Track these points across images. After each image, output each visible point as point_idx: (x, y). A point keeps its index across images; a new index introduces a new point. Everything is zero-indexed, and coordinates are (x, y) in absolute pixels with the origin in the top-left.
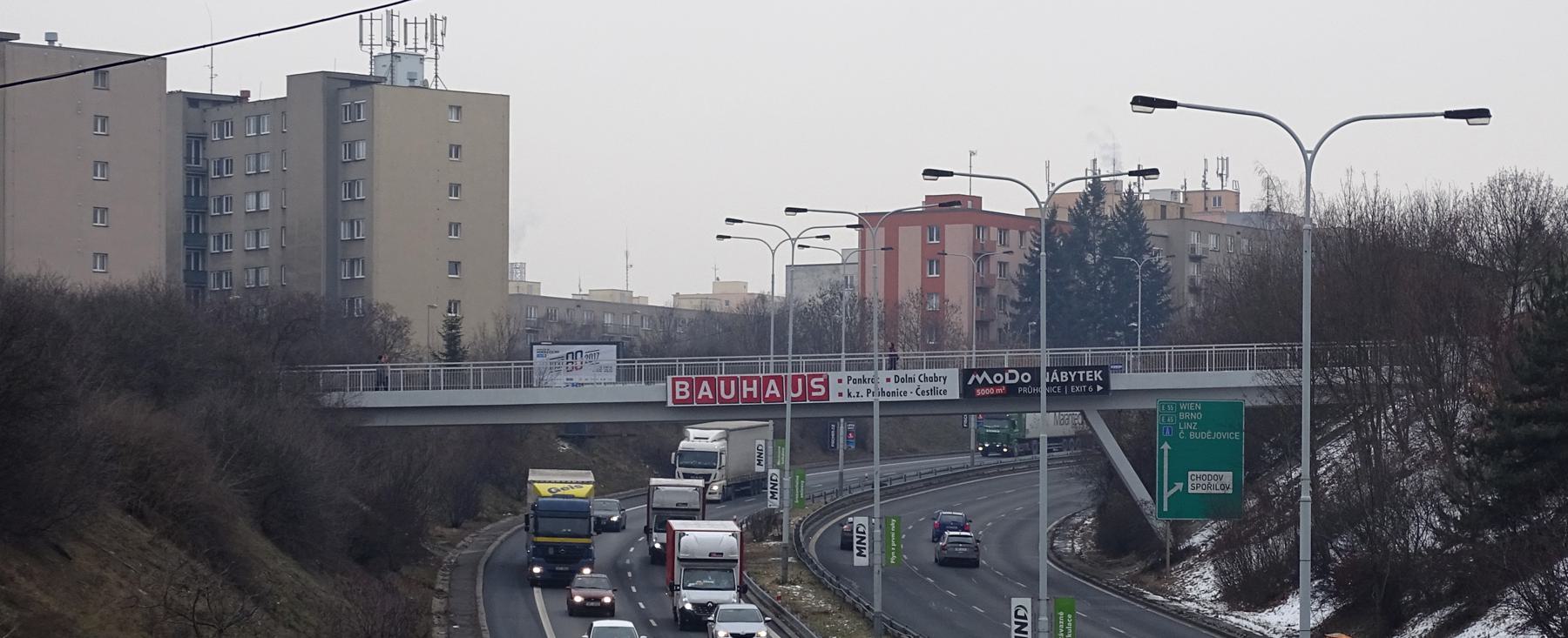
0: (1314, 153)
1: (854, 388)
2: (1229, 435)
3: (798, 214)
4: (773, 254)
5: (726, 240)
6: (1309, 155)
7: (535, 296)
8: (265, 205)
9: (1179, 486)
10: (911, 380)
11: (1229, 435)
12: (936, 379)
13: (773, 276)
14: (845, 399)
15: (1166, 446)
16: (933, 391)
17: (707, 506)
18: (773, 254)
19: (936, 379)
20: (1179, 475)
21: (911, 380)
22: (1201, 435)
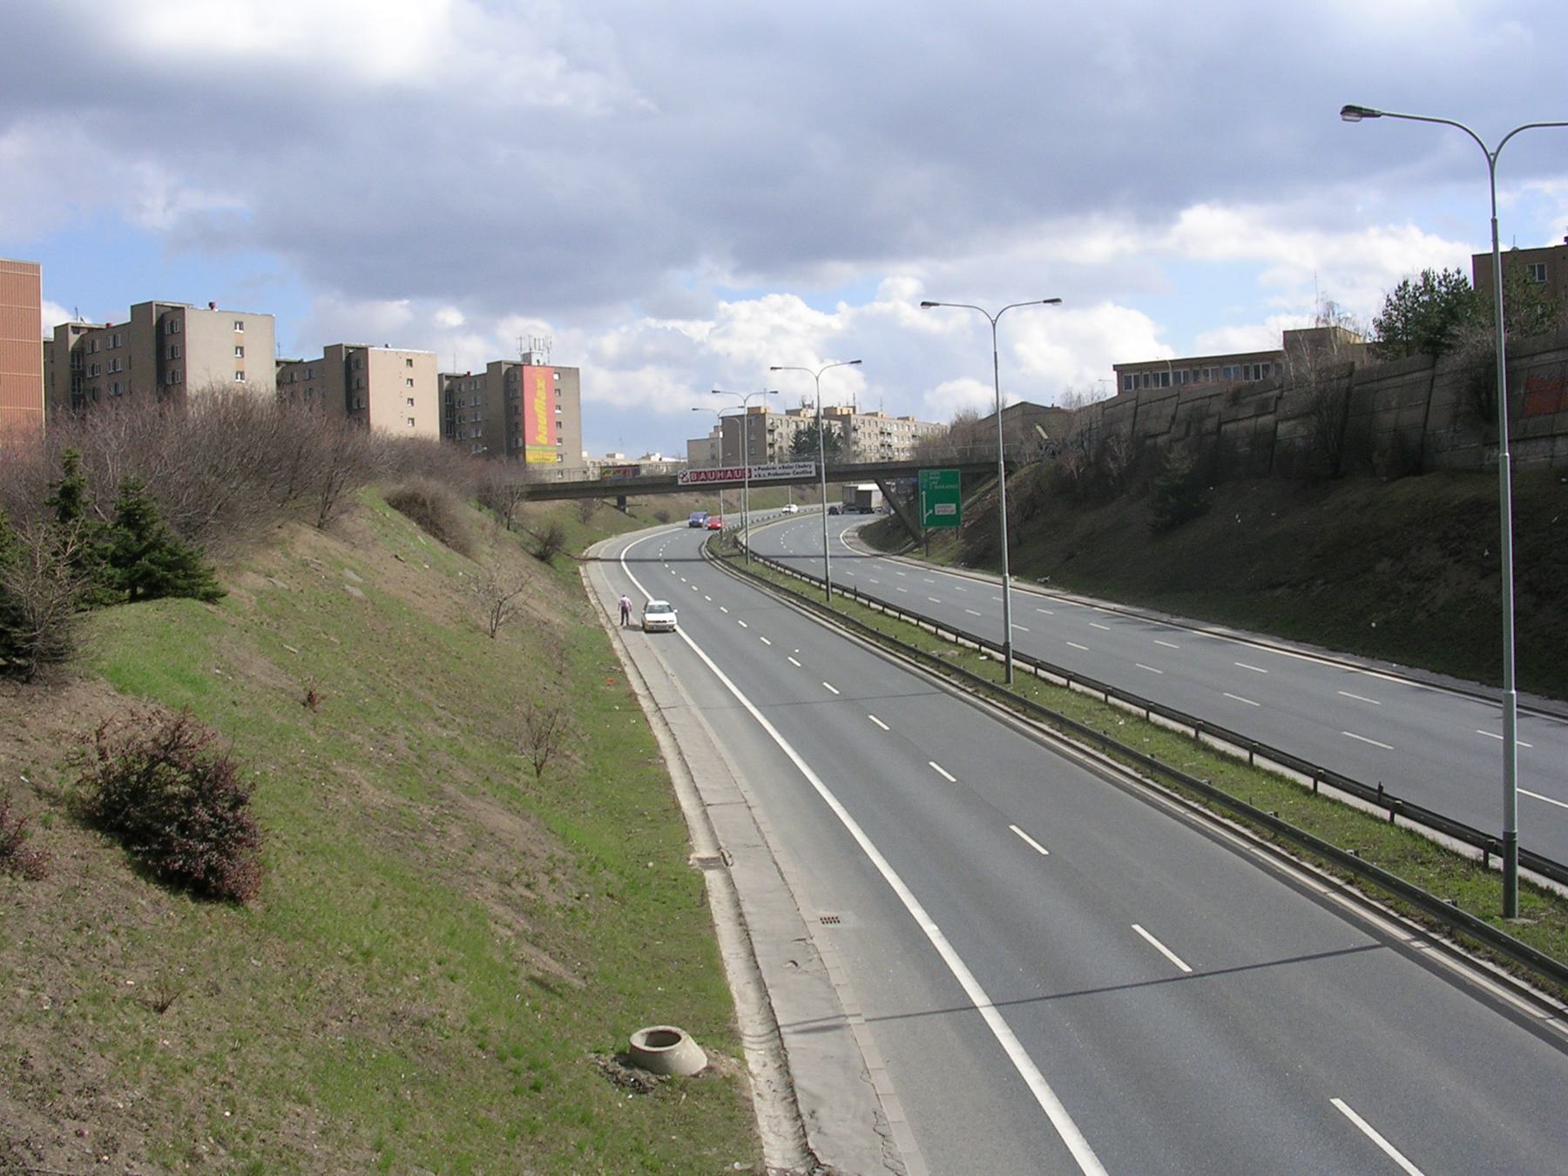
0: (1496, 155)
1: (762, 472)
2: (952, 487)
3: (1364, 119)
4: (994, 325)
5: (932, 307)
6: (1492, 157)
7: (581, 447)
8: (479, 419)
9: (931, 512)
10: (791, 467)
11: (952, 487)
12: (805, 466)
13: (995, 353)
14: (757, 478)
15: (924, 493)
16: (803, 472)
17: (823, 554)
18: (994, 325)
19: (805, 466)
20: (930, 506)
21: (791, 467)
22: (940, 487)
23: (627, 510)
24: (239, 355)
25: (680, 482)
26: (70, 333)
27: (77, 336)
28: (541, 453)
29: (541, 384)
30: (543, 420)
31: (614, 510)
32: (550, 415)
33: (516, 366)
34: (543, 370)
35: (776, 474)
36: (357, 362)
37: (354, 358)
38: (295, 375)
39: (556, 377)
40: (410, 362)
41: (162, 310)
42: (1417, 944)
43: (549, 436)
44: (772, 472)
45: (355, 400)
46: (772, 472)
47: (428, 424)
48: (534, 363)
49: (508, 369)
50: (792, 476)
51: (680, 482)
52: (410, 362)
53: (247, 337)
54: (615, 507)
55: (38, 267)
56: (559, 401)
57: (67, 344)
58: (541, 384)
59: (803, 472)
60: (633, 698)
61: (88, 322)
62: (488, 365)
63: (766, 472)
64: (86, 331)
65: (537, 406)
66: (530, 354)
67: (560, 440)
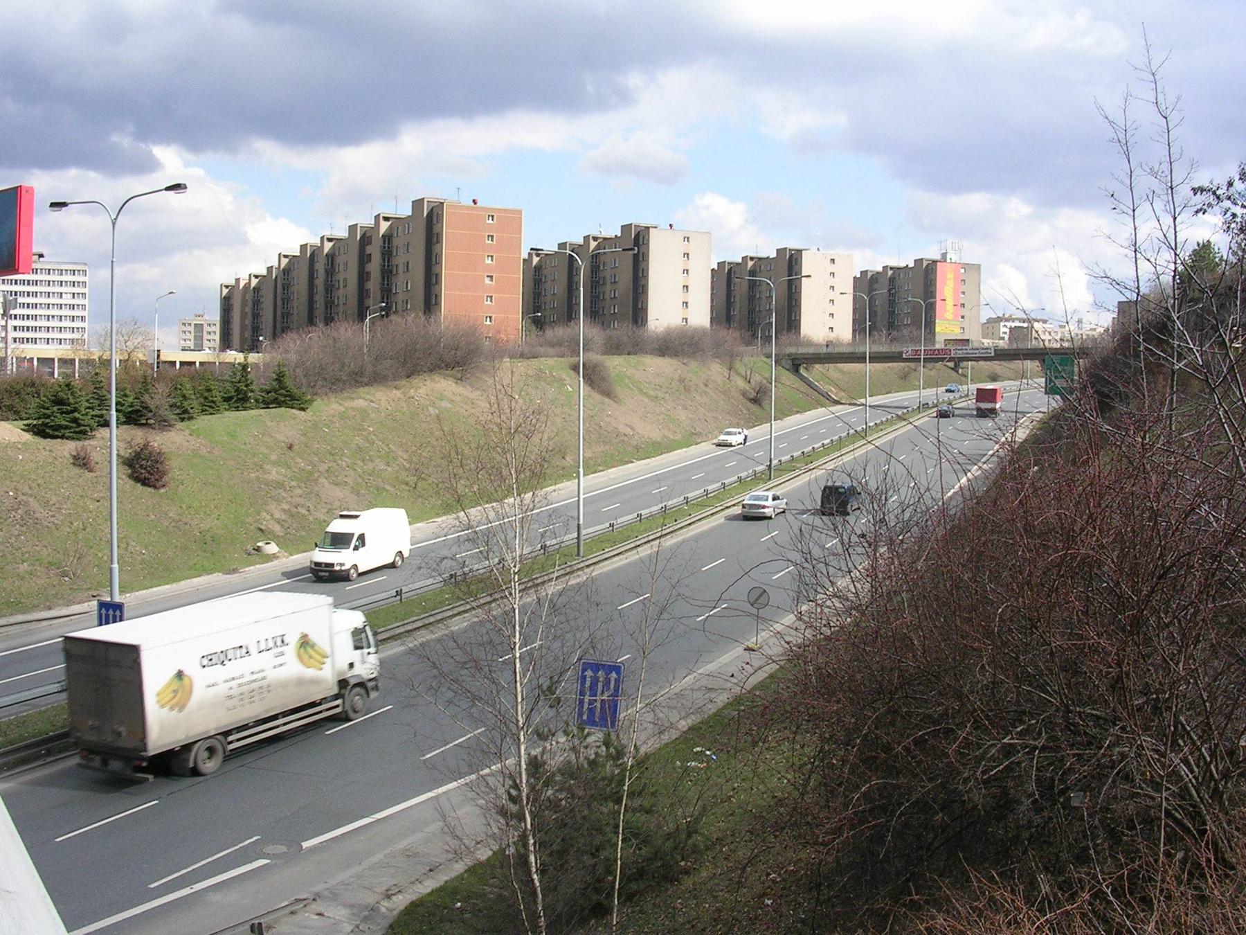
23: (960, 371)
24: (686, 258)
25: (904, 356)
26: (591, 241)
27: (596, 243)
28: (947, 327)
29: (950, 276)
30: (950, 302)
31: (950, 371)
32: (956, 297)
33: (935, 262)
34: (953, 266)
35: (968, 353)
36: (796, 259)
37: (795, 257)
38: (762, 267)
39: (963, 271)
40: (833, 261)
41: (639, 229)
42: (1173, 812)
43: (955, 315)
44: (965, 351)
45: (794, 287)
46: (965, 351)
47: (700, 315)
48: (948, 261)
49: (928, 265)
50: (978, 355)
51: (904, 356)
52: (833, 261)
53: (691, 248)
54: (952, 369)
55: (521, 212)
56: (963, 288)
57: (589, 248)
58: (950, 276)
59: (987, 353)
60: (120, 500)
61: (605, 234)
62: (915, 260)
63: (961, 352)
64: (601, 240)
65: (946, 289)
66: (946, 253)
67: (963, 317)
